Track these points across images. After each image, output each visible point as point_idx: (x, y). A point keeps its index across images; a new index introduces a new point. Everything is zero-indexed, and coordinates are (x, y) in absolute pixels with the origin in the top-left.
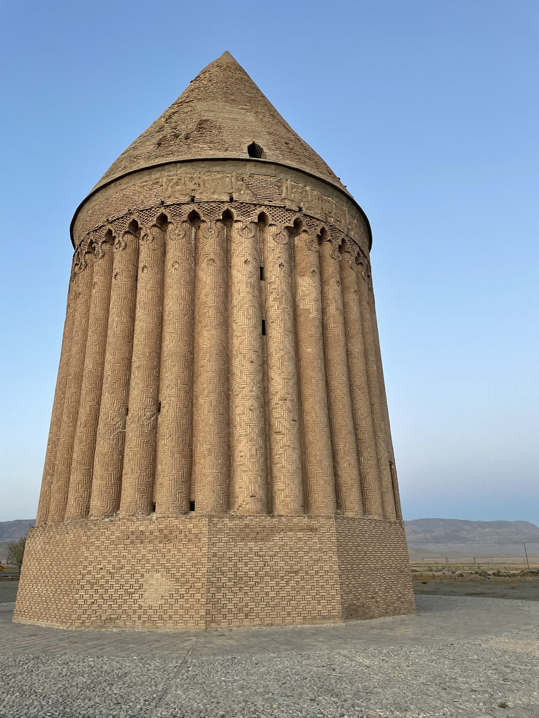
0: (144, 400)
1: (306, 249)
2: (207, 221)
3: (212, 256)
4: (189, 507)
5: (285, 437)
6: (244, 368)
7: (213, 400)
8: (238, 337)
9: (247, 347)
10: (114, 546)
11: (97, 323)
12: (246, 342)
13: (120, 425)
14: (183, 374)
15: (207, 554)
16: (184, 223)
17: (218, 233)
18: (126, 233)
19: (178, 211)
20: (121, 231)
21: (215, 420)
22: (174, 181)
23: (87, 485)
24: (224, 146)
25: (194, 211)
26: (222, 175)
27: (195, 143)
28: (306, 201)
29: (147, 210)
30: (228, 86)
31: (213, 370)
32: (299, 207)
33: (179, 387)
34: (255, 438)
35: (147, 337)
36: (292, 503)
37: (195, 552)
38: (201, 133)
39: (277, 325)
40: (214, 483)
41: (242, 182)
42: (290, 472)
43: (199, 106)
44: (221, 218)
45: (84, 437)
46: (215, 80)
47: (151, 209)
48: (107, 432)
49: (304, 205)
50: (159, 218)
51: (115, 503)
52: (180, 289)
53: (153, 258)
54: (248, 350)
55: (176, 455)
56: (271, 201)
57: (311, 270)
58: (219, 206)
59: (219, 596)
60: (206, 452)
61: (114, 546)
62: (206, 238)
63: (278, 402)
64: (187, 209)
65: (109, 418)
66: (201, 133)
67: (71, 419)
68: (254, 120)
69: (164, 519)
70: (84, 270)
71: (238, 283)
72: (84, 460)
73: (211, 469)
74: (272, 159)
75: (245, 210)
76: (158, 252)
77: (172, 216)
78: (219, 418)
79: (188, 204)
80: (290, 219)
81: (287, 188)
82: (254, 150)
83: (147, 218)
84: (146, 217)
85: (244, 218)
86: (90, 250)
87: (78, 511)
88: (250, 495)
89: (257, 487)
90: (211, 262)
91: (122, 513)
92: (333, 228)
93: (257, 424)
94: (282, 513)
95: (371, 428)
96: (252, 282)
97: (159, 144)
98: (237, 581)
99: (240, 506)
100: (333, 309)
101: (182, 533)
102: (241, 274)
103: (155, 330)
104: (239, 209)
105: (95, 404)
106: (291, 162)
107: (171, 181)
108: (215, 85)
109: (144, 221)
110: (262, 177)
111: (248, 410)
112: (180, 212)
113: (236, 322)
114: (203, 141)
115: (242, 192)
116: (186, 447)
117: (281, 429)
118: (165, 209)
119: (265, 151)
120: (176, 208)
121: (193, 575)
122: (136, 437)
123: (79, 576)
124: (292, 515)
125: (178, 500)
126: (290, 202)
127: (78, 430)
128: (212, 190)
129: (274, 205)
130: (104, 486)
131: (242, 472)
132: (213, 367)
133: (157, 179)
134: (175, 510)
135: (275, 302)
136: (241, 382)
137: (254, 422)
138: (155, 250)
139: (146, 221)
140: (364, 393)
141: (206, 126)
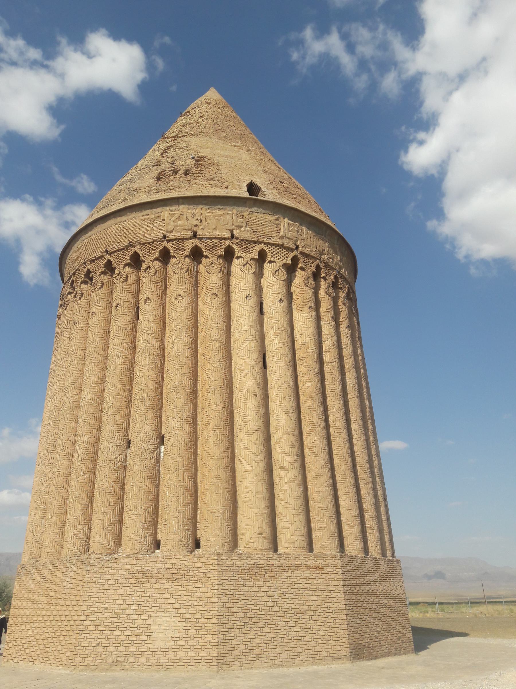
0: (147, 433)
1: (303, 285)
2: (210, 256)
3: (215, 290)
4: (194, 545)
5: (290, 472)
6: (247, 401)
7: (218, 434)
8: (241, 370)
9: (250, 380)
10: (118, 585)
11: (95, 353)
12: (249, 376)
13: (122, 458)
14: (188, 407)
15: (217, 593)
16: (187, 258)
17: (220, 268)
18: (127, 265)
19: (180, 246)
20: (122, 262)
21: (221, 455)
22: (176, 216)
23: (86, 521)
24: (224, 184)
25: (196, 246)
26: (223, 212)
27: (195, 179)
28: (302, 239)
29: (149, 243)
30: (219, 123)
31: (218, 403)
32: (295, 245)
33: (184, 420)
34: (261, 473)
35: (150, 369)
36: (298, 541)
37: (204, 591)
38: (200, 170)
39: (278, 359)
40: (221, 519)
41: (242, 220)
42: (296, 509)
43: (194, 141)
44: (223, 253)
45: (83, 470)
46: (206, 116)
47: (153, 243)
48: (108, 466)
49: (300, 243)
50: (161, 252)
51: (116, 540)
52: (183, 322)
53: (155, 290)
54: (252, 384)
55: (182, 490)
56: (270, 239)
57: (309, 305)
58: (221, 242)
59: (230, 636)
60: (212, 488)
61: (118, 585)
62: (208, 273)
63: (281, 436)
64: (189, 245)
65: (110, 451)
66: (200, 170)
67: (66, 451)
68: (248, 158)
69: (171, 557)
70: (80, 299)
71: (240, 317)
72: (82, 495)
73: (218, 505)
74: (271, 198)
75: (245, 246)
76: (160, 285)
77: (175, 251)
78: (225, 453)
79: (190, 239)
80: (287, 256)
81: (284, 226)
82: (252, 188)
83: (148, 251)
84: (148, 249)
85: (245, 254)
86: (86, 279)
87: (76, 548)
88: (258, 532)
89: (264, 523)
90: (214, 296)
91: (125, 550)
92: (327, 265)
93: (262, 459)
94: (288, 551)
95: (368, 464)
96: (254, 316)
97: (158, 179)
98: (248, 621)
99: (247, 545)
100: (328, 344)
101: (190, 572)
102: (243, 309)
103: (158, 362)
104: (240, 246)
105: (93, 436)
106: (288, 201)
107: (173, 216)
108: (206, 121)
109: (145, 254)
110: (261, 215)
111: (253, 444)
112: (183, 246)
113: (238, 355)
114: (203, 178)
115: (243, 229)
116: (192, 483)
117: (285, 464)
118: (167, 243)
119: (263, 190)
120: (178, 242)
121: (203, 615)
122: (140, 472)
123: (83, 617)
124: (299, 553)
125: (185, 538)
126: (287, 239)
127: (76, 464)
128: (214, 227)
129: (273, 242)
130: (106, 523)
131: (248, 509)
132: (218, 400)
133: (158, 213)
134: (182, 548)
135: (275, 336)
136: (245, 415)
137: (259, 457)
138: (157, 283)
139: (148, 253)
140: (360, 428)
141: (204, 163)
